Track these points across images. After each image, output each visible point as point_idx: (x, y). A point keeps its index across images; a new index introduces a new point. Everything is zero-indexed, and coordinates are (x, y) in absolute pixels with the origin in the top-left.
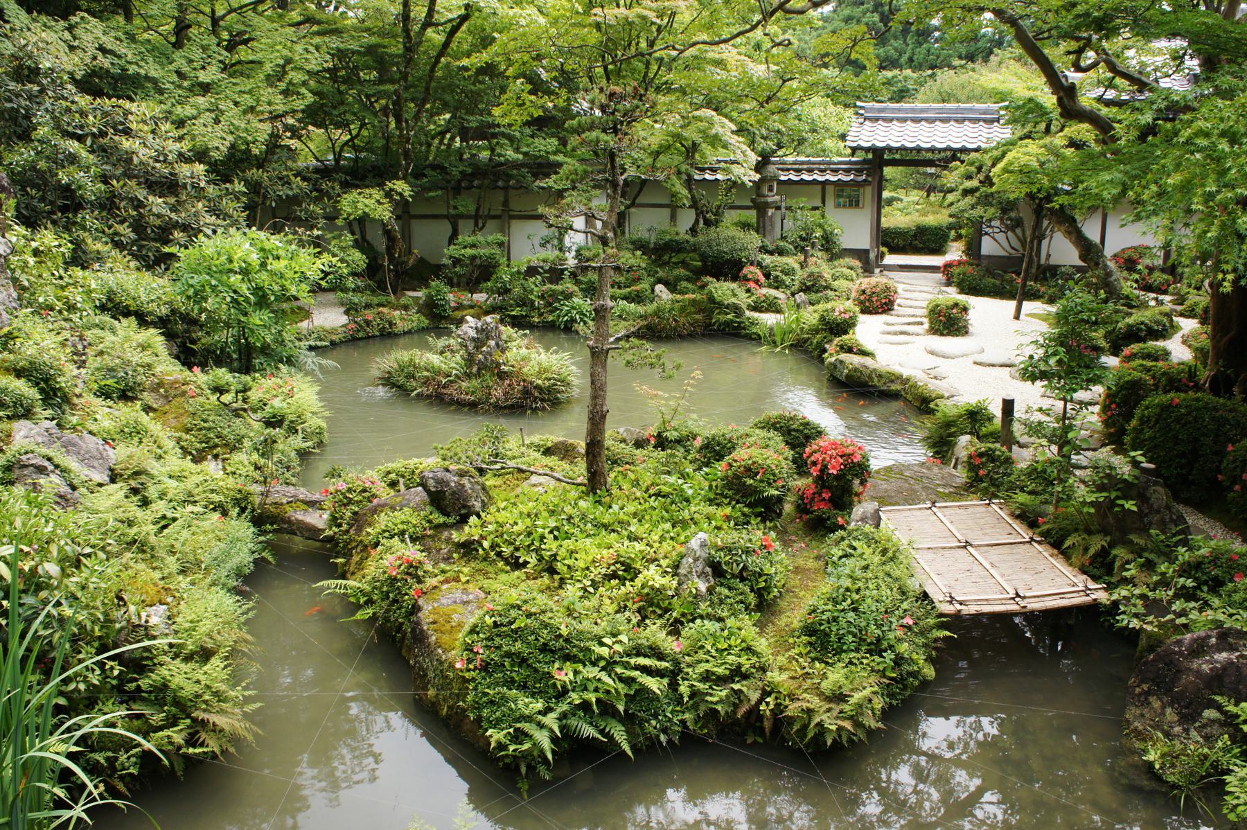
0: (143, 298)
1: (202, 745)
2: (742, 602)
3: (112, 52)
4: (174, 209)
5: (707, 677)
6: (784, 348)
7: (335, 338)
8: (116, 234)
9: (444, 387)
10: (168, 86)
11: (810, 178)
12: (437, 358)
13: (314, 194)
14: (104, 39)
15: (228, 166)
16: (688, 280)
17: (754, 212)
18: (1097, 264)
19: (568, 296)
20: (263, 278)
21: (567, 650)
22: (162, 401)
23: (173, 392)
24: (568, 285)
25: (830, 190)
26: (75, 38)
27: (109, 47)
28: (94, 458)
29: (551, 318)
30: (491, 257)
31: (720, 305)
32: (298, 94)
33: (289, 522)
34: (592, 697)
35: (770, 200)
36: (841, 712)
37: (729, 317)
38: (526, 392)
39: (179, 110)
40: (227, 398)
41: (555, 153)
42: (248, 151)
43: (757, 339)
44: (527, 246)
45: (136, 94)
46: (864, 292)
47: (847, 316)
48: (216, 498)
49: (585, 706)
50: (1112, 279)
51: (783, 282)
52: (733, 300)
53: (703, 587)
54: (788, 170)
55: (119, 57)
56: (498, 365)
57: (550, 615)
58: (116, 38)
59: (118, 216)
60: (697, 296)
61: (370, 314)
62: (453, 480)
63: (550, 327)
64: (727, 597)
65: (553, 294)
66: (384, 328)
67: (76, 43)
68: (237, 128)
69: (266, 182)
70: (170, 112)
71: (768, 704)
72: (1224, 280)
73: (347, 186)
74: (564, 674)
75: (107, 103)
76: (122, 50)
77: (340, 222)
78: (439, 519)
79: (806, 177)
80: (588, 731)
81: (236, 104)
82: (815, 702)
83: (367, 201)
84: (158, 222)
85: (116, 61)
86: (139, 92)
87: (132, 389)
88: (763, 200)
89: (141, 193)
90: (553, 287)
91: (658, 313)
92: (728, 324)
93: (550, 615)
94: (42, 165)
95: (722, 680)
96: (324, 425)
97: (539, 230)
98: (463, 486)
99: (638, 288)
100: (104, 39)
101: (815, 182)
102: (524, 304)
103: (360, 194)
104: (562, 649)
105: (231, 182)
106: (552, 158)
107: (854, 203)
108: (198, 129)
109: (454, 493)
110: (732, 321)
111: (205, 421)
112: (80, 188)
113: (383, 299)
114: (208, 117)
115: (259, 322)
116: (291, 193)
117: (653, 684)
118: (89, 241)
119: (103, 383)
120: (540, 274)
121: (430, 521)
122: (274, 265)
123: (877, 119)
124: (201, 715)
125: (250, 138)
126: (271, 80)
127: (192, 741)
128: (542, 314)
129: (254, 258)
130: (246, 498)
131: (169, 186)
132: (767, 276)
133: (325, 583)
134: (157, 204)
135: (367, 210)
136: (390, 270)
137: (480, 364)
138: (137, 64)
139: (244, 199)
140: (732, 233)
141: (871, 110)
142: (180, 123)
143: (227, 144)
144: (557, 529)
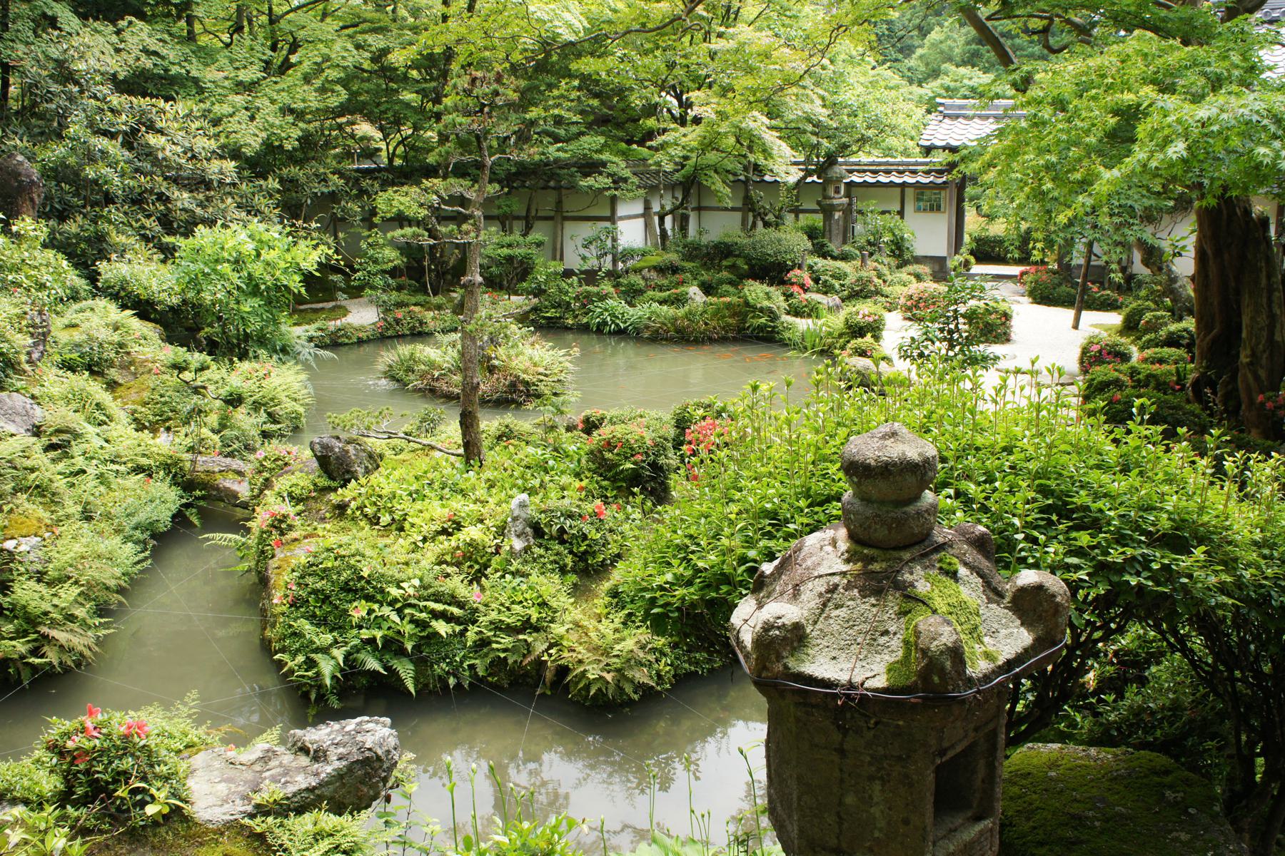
0: (155, 288)
1: (42, 656)
2: (556, 562)
3: (156, 53)
4: (200, 205)
5: (497, 626)
6: (813, 353)
7: (363, 335)
8: (143, 227)
9: (438, 379)
10: (209, 85)
11: (887, 180)
12: (439, 354)
13: (354, 192)
14: (148, 40)
15: (257, 165)
16: (731, 283)
17: (821, 216)
18: (1160, 269)
19: (603, 298)
20: (257, 269)
21: (357, 588)
22: (131, 377)
23: (141, 370)
24: (607, 287)
25: (910, 193)
26: (122, 41)
27: (152, 48)
28: (18, 414)
29: (585, 320)
30: (528, 257)
31: (754, 308)
32: (333, 91)
33: (218, 489)
34: (379, 634)
35: (835, 202)
36: (608, 665)
37: (763, 320)
38: (513, 386)
39: (217, 109)
40: (187, 376)
41: (599, 151)
42: (281, 146)
43: (784, 344)
44: (578, 247)
45: (177, 94)
46: (911, 297)
47: (871, 319)
48: (144, 461)
49: (372, 641)
50: (1177, 285)
51: (832, 287)
52: (766, 303)
53: (518, 545)
54: (864, 171)
55: (163, 58)
56: (490, 359)
57: (358, 558)
58: (160, 40)
59: (145, 210)
60: (735, 300)
61: (400, 313)
62: (337, 446)
63: (585, 329)
64: (541, 556)
65: (588, 296)
66: (414, 327)
67: (122, 46)
68: (272, 126)
69: (303, 180)
70: (209, 111)
71: (550, 655)
72: (1034, 248)
73: (385, 185)
74: (359, 610)
75: (144, 102)
76: (164, 52)
77: (376, 220)
78: (324, 482)
79: (883, 179)
80: (373, 664)
81: (273, 102)
82: (582, 652)
83: (402, 199)
84: (184, 216)
85: (159, 62)
86: (181, 91)
87: (98, 364)
88: (828, 202)
89: (163, 187)
90: (590, 288)
91: (689, 316)
92: (761, 328)
93: (358, 558)
94: (72, 160)
95: (511, 630)
96: (301, 410)
97: (588, 230)
98: (347, 452)
99: (678, 291)
100: (148, 40)
101: (892, 184)
102: (559, 306)
103: (396, 192)
104: (363, 589)
105: (266, 179)
106: (596, 156)
107: (935, 208)
108: (232, 125)
109: (338, 458)
110: (766, 326)
111: (162, 396)
112: (106, 183)
113: (420, 298)
114: (244, 115)
115: (248, 309)
116: (326, 190)
117: (442, 628)
118: (114, 234)
119: (68, 356)
120: (576, 275)
121: (315, 485)
122: (268, 255)
123: (957, 117)
124: (44, 629)
125: (283, 135)
126: (307, 79)
127: (35, 652)
128: (576, 317)
129: (249, 247)
130: (176, 464)
131: (199, 183)
132: (816, 281)
133: (211, 535)
134: (183, 199)
135: (402, 208)
136: (430, 270)
137: (476, 360)
138: (179, 64)
139: (278, 196)
140: (791, 238)
141: (952, 107)
142: (216, 122)
143: (260, 140)
144: (417, 492)
